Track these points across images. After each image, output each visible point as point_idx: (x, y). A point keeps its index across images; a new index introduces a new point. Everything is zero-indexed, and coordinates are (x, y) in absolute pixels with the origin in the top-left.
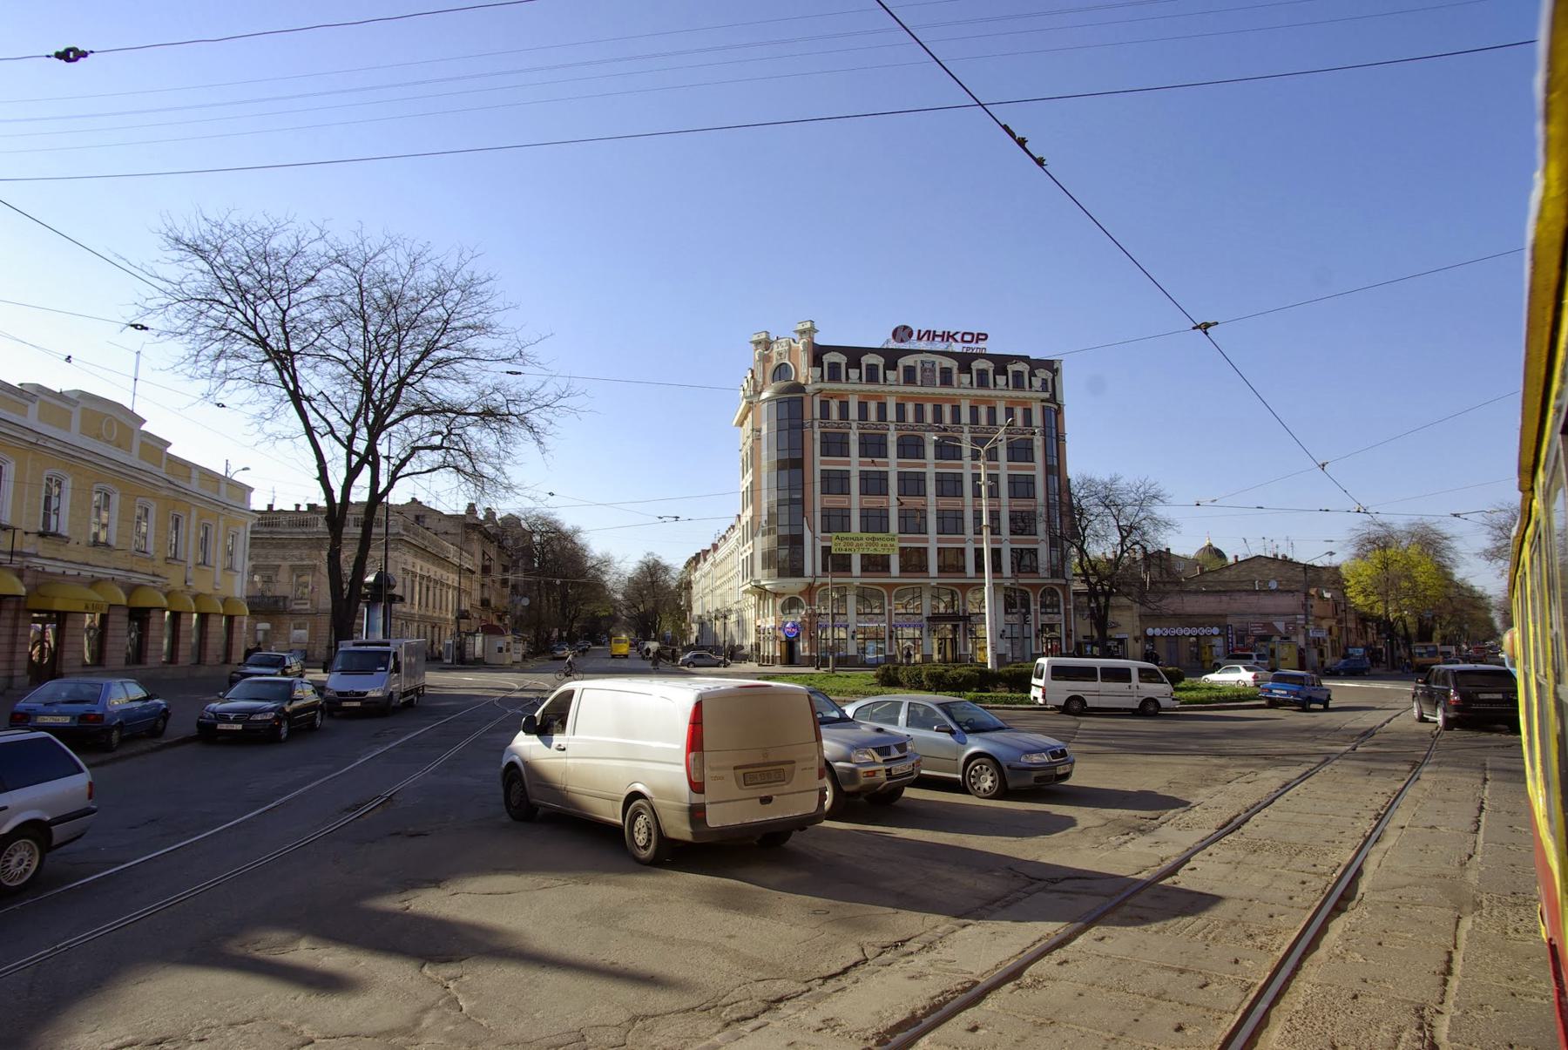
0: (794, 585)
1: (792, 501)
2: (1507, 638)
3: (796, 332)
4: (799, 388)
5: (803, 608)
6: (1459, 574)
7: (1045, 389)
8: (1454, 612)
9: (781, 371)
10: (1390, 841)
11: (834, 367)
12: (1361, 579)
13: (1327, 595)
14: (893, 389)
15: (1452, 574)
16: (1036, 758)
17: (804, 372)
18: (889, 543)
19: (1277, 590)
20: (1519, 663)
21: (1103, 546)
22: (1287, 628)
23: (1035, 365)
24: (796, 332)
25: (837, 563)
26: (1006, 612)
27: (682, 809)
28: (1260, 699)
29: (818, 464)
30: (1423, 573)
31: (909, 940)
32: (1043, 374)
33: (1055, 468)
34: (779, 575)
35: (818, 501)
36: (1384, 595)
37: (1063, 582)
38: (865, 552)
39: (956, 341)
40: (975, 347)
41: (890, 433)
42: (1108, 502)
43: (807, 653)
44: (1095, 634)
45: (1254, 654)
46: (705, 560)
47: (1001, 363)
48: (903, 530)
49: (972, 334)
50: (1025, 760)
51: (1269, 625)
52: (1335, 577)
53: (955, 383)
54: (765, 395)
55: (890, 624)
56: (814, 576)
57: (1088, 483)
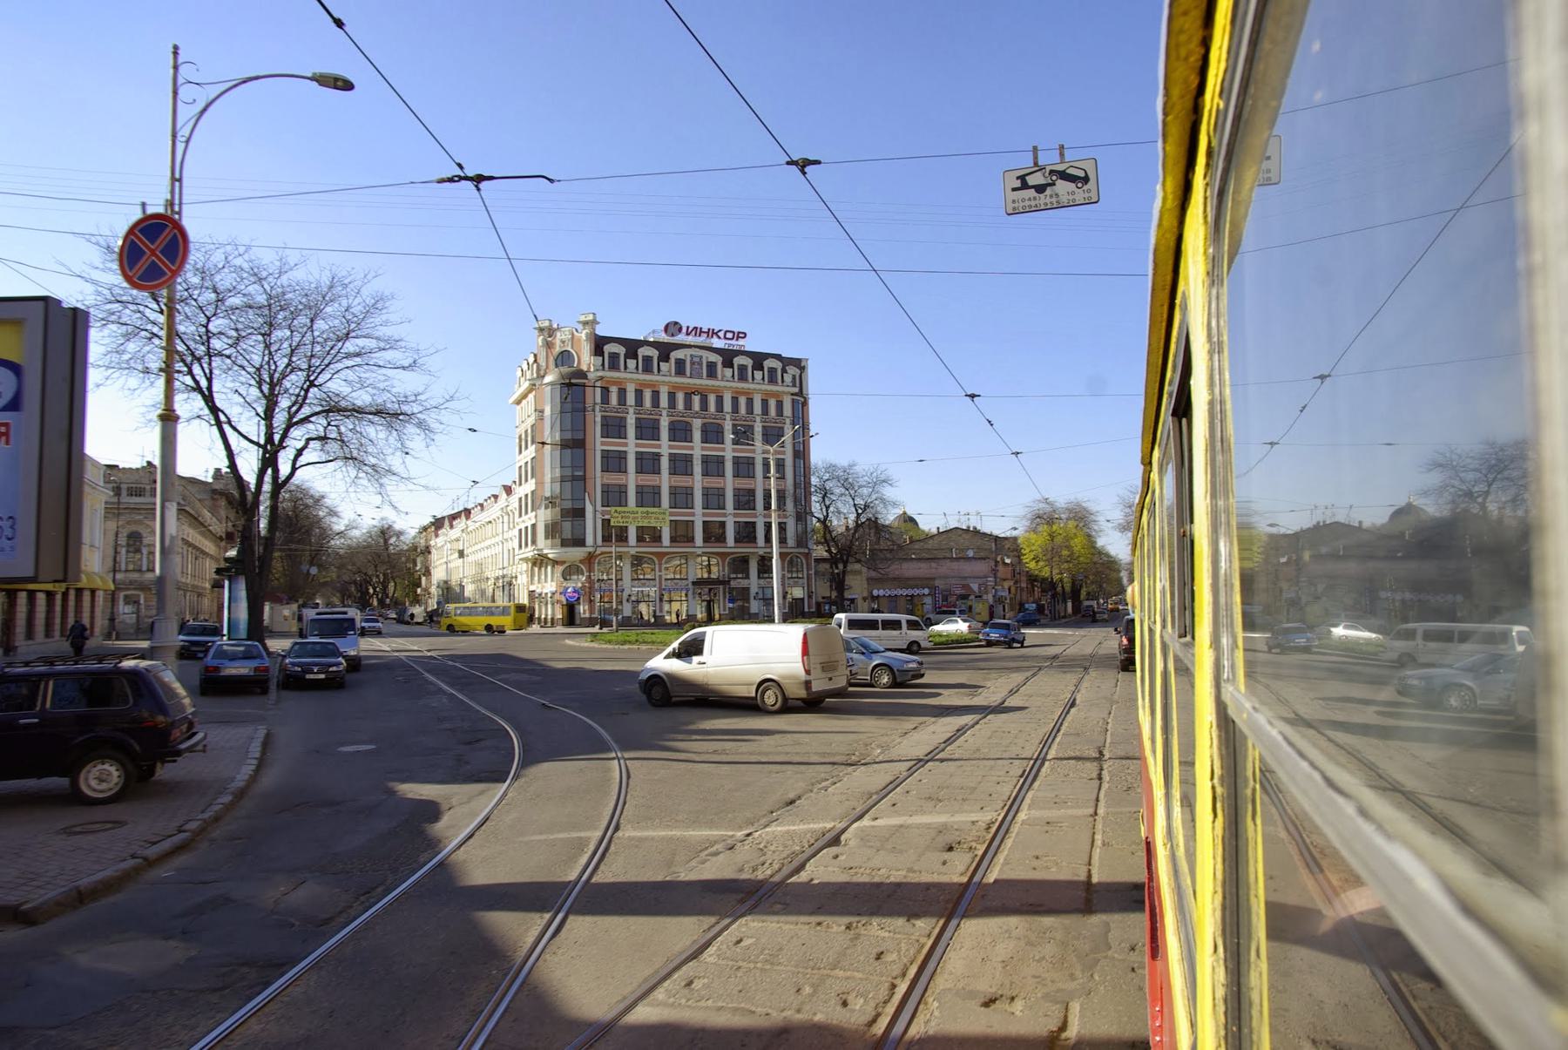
0: (576, 553)
1: (575, 478)
2: (1129, 590)
3: (579, 322)
4: (582, 374)
5: (583, 574)
6: (1100, 542)
7: (794, 386)
8: (1097, 573)
9: (564, 358)
10: (1083, 691)
11: (614, 357)
12: (1033, 548)
13: (1008, 561)
14: (758, 387)
15: (1095, 542)
16: (911, 665)
17: (586, 359)
18: (661, 517)
19: (973, 558)
20: (1137, 610)
21: (843, 518)
22: (980, 588)
23: (787, 362)
24: (579, 322)
25: (614, 534)
26: (759, 577)
27: (800, 683)
28: (981, 641)
29: (598, 444)
30: (1078, 543)
31: (799, 798)
32: (792, 370)
33: (801, 454)
34: (562, 545)
35: (598, 477)
36: (1050, 562)
37: (806, 551)
38: (640, 525)
39: (719, 337)
40: (736, 344)
41: (662, 419)
42: (848, 485)
43: (587, 615)
44: (834, 594)
45: (957, 610)
46: (451, 527)
47: (759, 359)
48: (673, 505)
49: (734, 332)
50: (906, 667)
51: (965, 586)
52: (1015, 546)
53: (720, 377)
54: (548, 379)
55: (660, 587)
56: (595, 545)
57: (831, 468)
